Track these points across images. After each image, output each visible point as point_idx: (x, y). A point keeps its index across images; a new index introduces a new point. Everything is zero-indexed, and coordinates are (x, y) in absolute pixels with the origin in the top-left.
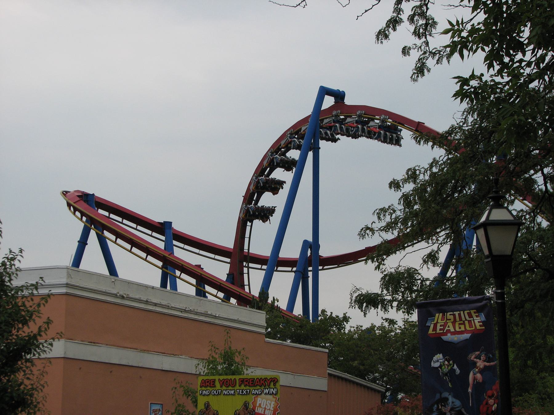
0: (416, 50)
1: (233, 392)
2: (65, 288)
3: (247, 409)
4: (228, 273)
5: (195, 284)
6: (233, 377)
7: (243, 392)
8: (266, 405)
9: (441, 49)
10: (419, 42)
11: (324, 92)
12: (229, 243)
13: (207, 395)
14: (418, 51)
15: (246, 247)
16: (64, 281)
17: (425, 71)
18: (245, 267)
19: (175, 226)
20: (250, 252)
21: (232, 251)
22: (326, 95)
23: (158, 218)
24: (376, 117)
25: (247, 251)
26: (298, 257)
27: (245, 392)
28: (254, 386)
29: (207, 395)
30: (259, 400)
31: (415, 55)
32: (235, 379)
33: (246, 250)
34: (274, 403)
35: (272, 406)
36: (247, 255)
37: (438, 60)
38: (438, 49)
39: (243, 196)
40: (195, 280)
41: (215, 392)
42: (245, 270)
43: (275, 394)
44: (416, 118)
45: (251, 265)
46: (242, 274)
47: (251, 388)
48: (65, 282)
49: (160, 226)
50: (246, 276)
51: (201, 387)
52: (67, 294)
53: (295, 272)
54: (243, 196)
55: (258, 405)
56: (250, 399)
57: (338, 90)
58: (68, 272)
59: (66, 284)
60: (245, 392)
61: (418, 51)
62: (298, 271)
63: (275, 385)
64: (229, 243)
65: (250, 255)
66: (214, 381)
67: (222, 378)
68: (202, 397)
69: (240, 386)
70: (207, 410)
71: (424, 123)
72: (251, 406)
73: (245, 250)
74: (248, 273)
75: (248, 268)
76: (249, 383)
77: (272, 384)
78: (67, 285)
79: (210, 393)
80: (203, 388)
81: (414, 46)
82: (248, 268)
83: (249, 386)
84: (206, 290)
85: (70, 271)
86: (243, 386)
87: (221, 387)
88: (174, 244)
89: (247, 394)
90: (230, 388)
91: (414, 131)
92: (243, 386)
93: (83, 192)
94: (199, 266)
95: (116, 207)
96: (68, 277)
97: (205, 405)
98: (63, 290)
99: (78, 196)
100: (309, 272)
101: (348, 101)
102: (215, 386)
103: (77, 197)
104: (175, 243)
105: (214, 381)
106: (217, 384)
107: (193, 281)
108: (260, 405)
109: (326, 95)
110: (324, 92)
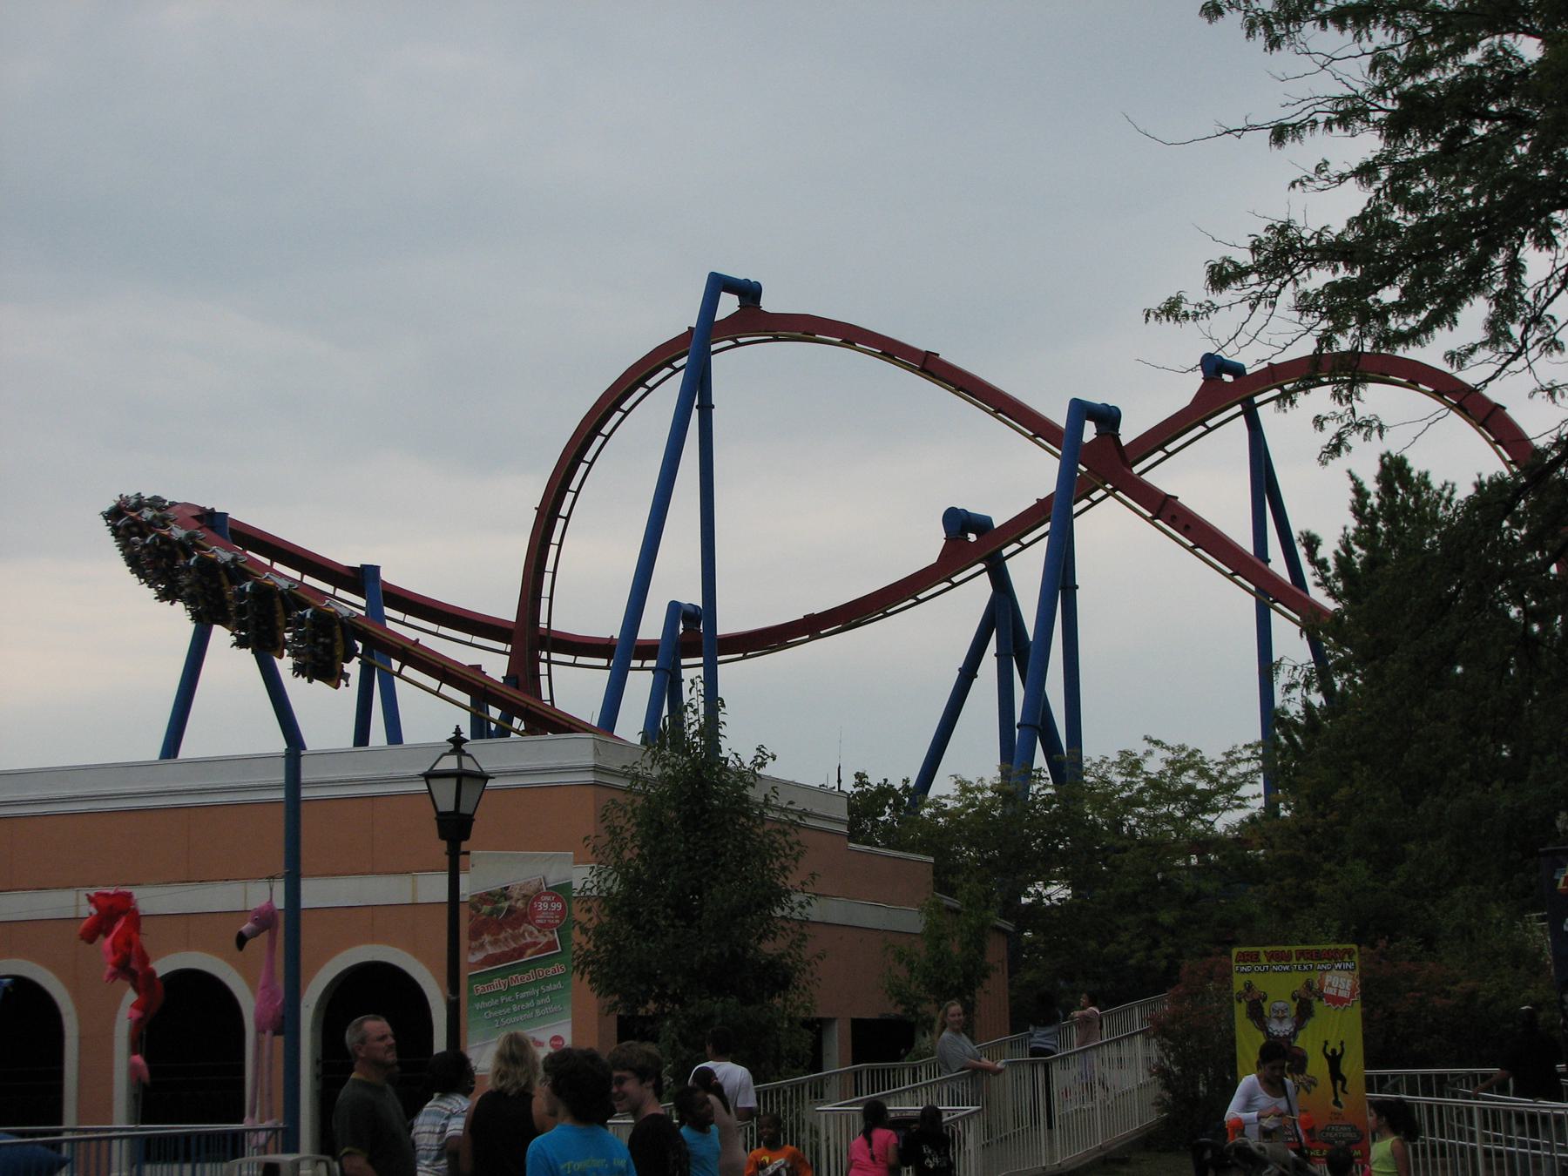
0: (1335, 420)
1: (1287, 968)
2: (590, 774)
3: (1310, 990)
4: (505, 675)
5: (469, 705)
6: (1286, 949)
7: (1302, 967)
8: (1339, 983)
9: (1371, 419)
10: (1340, 410)
11: (718, 284)
12: (506, 609)
13: (1247, 972)
14: (1338, 423)
15: (543, 618)
16: (589, 760)
17: (1343, 449)
18: (544, 661)
19: (386, 576)
20: (552, 628)
21: (512, 627)
22: (723, 293)
23: (349, 557)
24: (817, 336)
25: (546, 626)
26: (660, 638)
27: (1305, 967)
28: (1321, 959)
29: (1247, 972)
30: (1328, 978)
31: (1332, 428)
32: (1289, 951)
33: (543, 626)
34: (1351, 981)
35: (1349, 984)
36: (546, 635)
37: (1366, 434)
38: (1367, 419)
39: (536, 508)
40: (469, 696)
41: (1260, 968)
42: (543, 667)
43: (1352, 970)
44: (923, 345)
45: (555, 656)
46: (537, 676)
47: (1316, 963)
48: (592, 763)
49: (352, 575)
50: (544, 681)
51: (1237, 961)
52: (596, 784)
53: (653, 670)
54: (536, 508)
55: (1327, 984)
56: (1315, 977)
57: (757, 282)
58: (594, 743)
59: (594, 767)
60: (1305, 967)
61: (1338, 423)
62: (662, 669)
63: (1350, 957)
64: (506, 609)
65: (552, 635)
66: (1257, 954)
67: (1269, 949)
68: (1240, 975)
69: (1298, 959)
70: (1249, 991)
71: (938, 355)
72: (1316, 986)
73: (541, 626)
74: (549, 675)
75: (549, 662)
76: (1312, 955)
77: (1347, 956)
78: (596, 769)
79: (1253, 969)
80: (1241, 964)
81: (1332, 415)
82: (549, 662)
83: (1312, 960)
84: (491, 715)
85: (598, 742)
86: (1302, 959)
87: (1269, 961)
88: (386, 614)
89: (1309, 970)
90: (1283, 962)
91: (919, 370)
92: (1302, 959)
93: (202, 509)
94: (478, 668)
95: (258, 536)
96: (595, 755)
97: (1245, 985)
98: (589, 778)
99: (194, 517)
100: (682, 670)
101: (769, 304)
102: (1259, 961)
103: (192, 520)
104: (388, 611)
105: (1257, 954)
106: (1263, 958)
107: (465, 699)
108: (1330, 985)
109: (723, 293)
110: (718, 284)
